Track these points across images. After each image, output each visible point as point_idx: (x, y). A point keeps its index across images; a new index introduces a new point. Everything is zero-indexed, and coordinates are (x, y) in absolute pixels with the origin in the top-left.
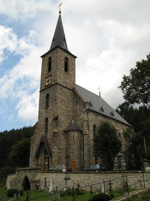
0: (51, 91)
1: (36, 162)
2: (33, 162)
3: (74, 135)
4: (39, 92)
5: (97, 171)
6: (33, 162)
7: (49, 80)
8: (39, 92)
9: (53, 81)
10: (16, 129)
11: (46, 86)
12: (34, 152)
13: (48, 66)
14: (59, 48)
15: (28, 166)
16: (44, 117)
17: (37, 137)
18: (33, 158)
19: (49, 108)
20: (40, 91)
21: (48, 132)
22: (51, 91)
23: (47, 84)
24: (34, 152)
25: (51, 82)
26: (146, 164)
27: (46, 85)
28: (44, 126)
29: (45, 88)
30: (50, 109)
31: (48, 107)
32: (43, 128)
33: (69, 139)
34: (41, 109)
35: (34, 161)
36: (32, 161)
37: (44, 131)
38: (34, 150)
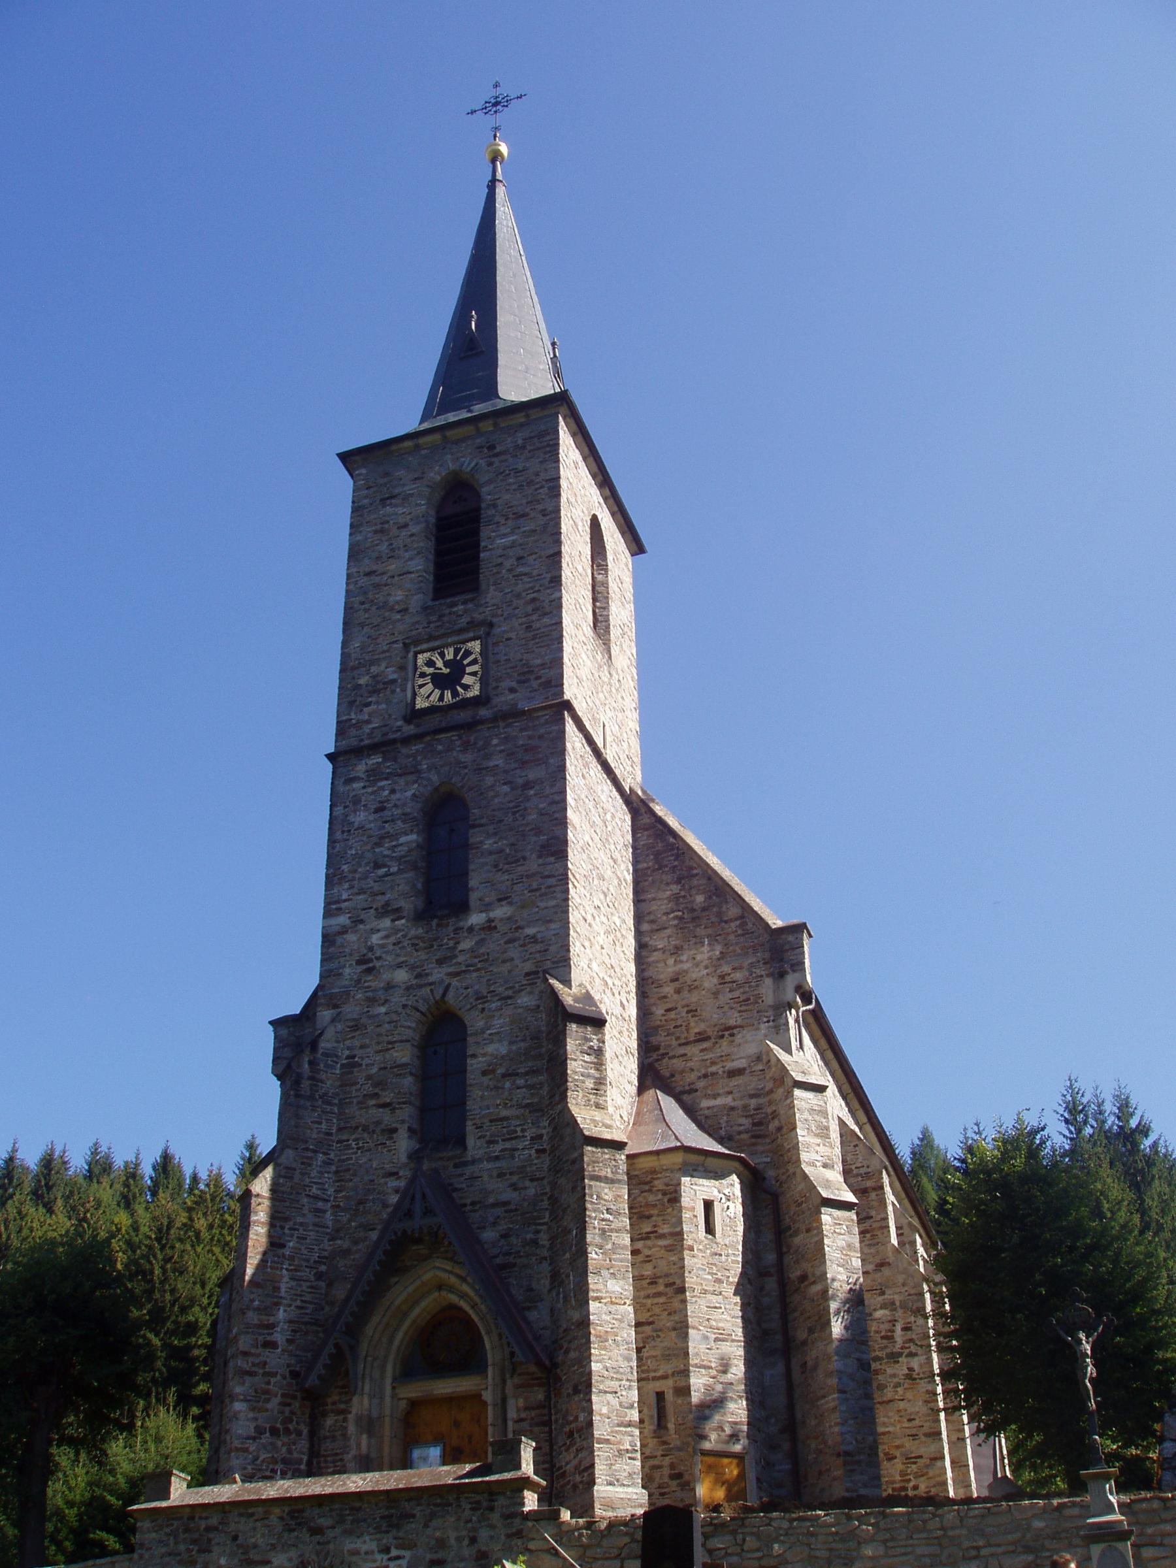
0: (498, 761)
1: (304, 1444)
2: (266, 1438)
3: (708, 1205)
4: (330, 757)
5: (599, 578)
6: (266, 1438)
7: (457, 668)
8: (330, 757)
9: (506, 684)
10: (950, 1146)
11: (414, 715)
12: (279, 1337)
13: (431, 545)
14: (1145, 1548)
15: (166, 1495)
16: (397, 998)
17: (314, 1190)
18: (274, 1404)
19: (476, 919)
20: (331, 749)
21: (471, 1141)
22: (498, 761)
23: (427, 696)
24: (279, 1337)
25: (484, 682)
26: (544, 1017)
27: (420, 704)
28: (410, 1079)
29: (410, 729)
30: (490, 926)
31: (462, 908)
32: (388, 1097)
33: (665, 1229)
34: (358, 921)
35: (274, 1432)
36: (260, 1431)
37: (410, 1129)
38: (281, 1314)
